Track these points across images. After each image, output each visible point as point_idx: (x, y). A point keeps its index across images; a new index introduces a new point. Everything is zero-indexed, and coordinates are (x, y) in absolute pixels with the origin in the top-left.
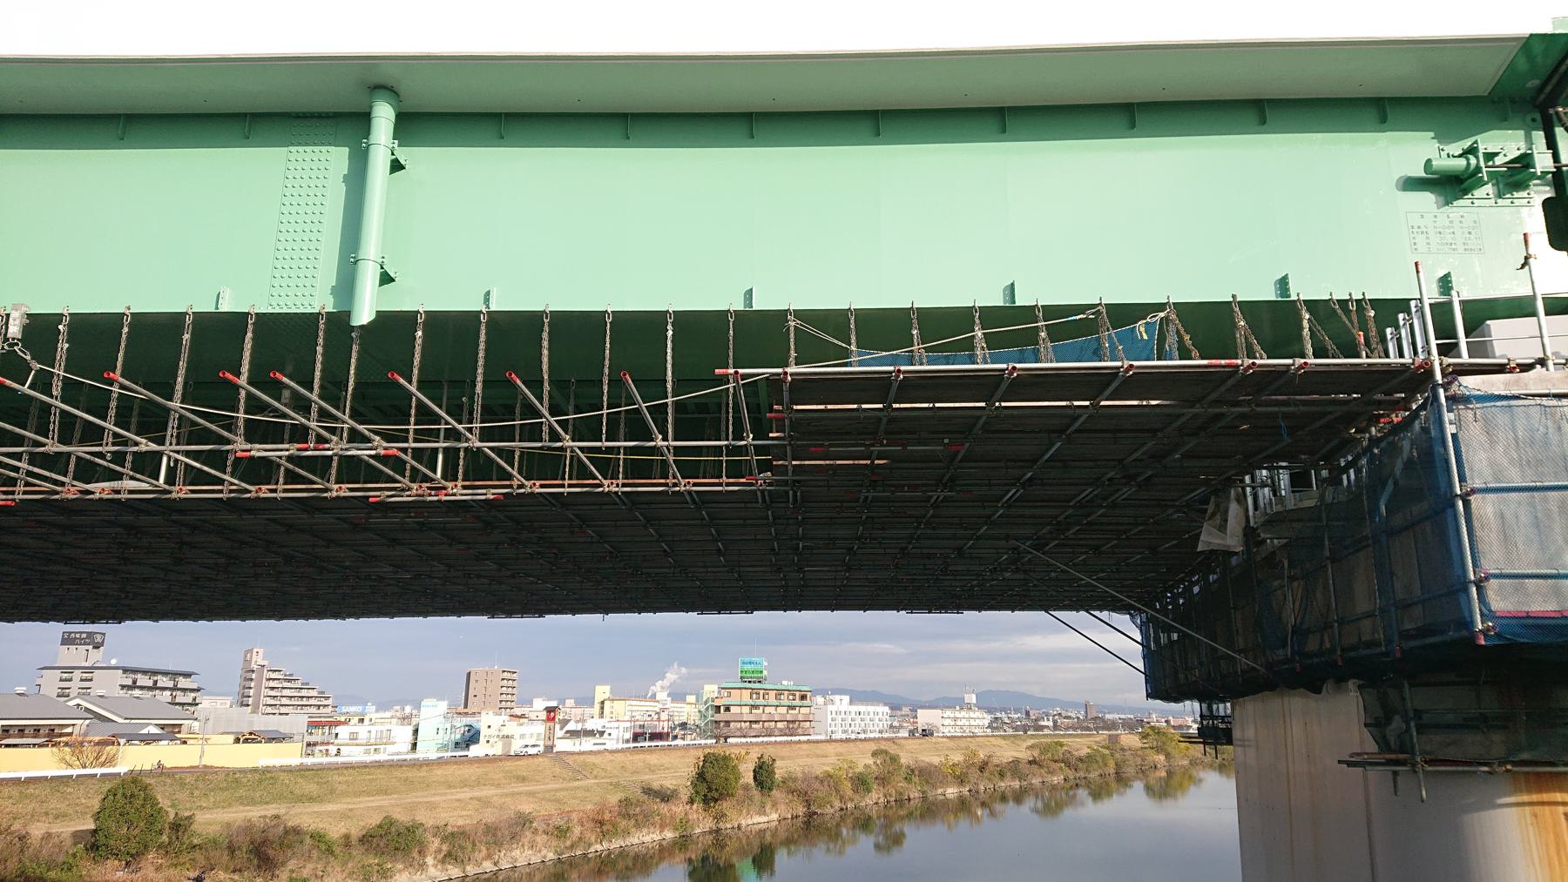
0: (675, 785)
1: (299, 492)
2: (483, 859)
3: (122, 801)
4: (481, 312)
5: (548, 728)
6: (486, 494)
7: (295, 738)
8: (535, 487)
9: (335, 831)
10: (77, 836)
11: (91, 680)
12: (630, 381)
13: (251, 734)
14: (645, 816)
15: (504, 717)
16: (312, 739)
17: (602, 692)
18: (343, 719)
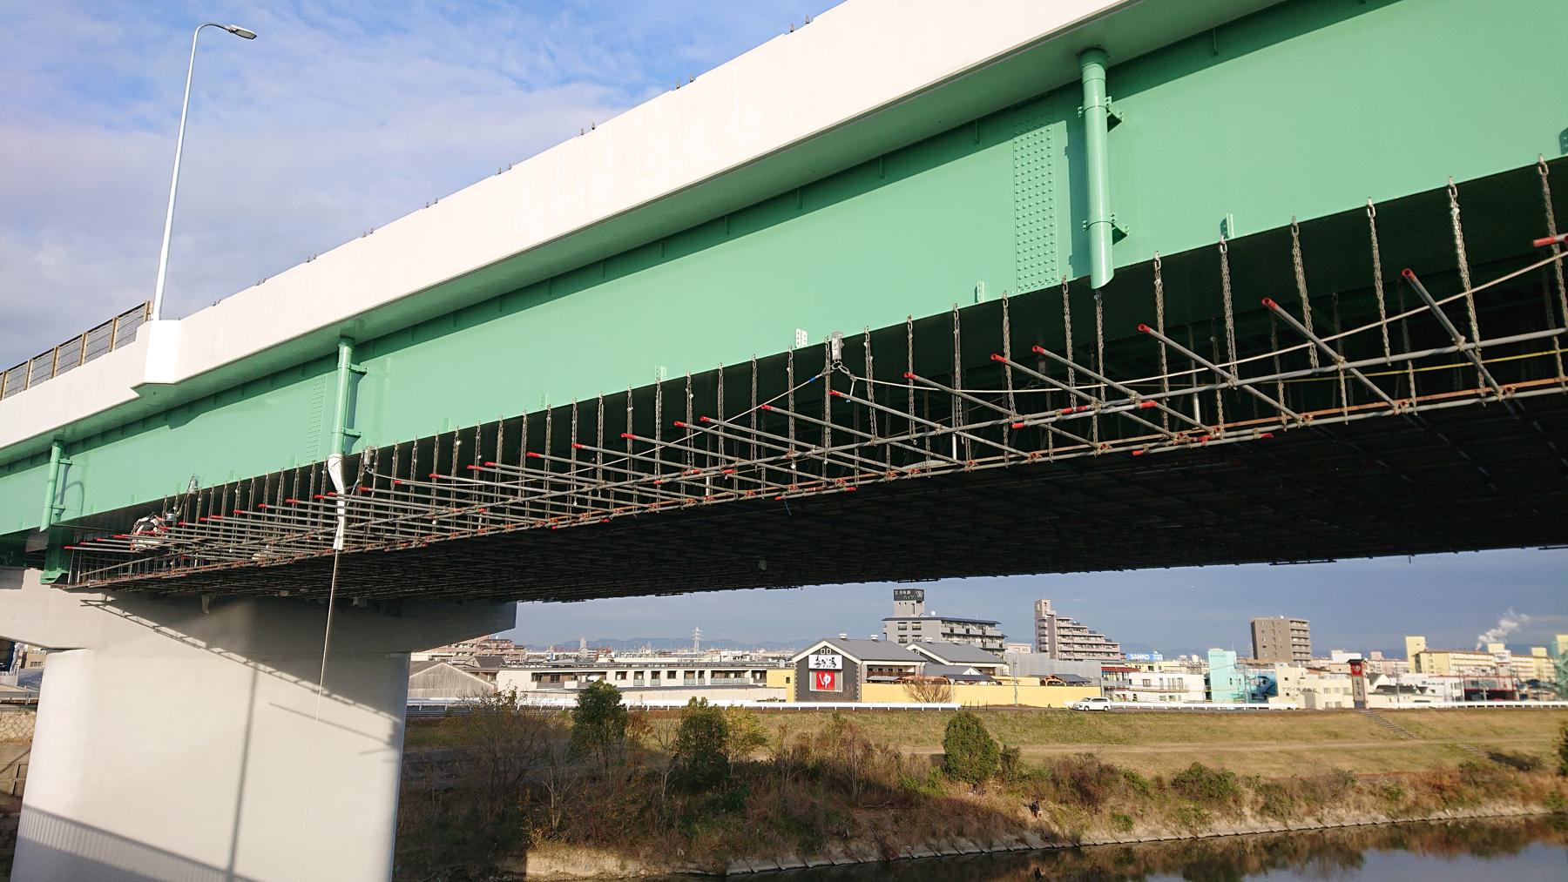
1: (1067, 453)
3: (961, 732)
5: (1355, 682)
6: (1253, 434)
7: (1093, 682)
8: (1308, 419)
9: (1147, 773)
10: (933, 757)
11: (920, 629)
12: (1416, 279)
13: (1053, 677)
14: (1498, 785)
15: (1300, 670)
16: (1108, 684)
17: (1415, 644)
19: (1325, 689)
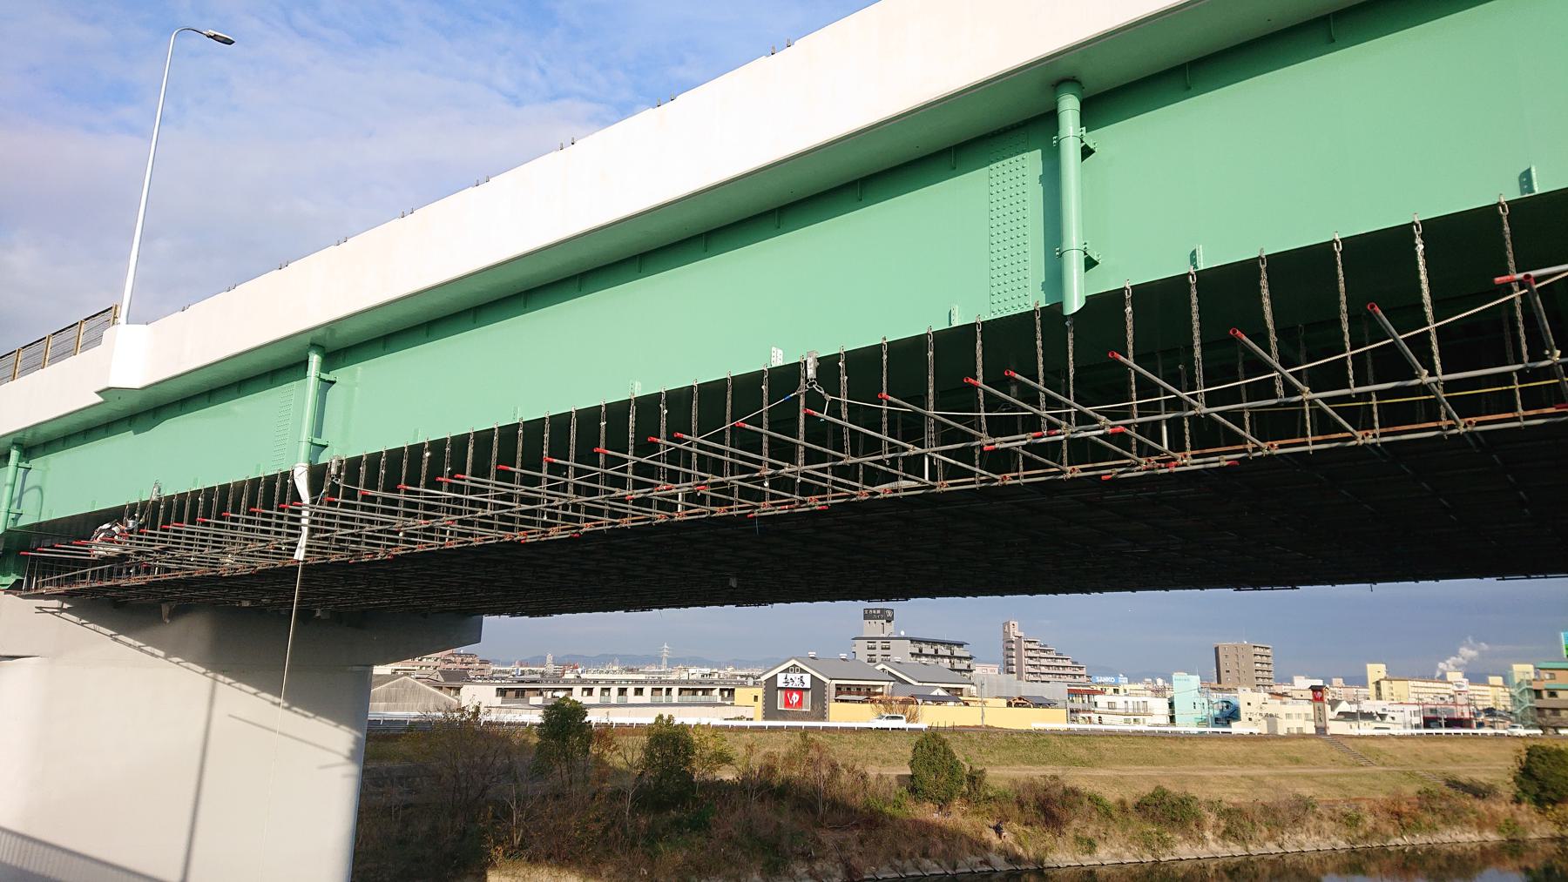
0: (1491, 780)
1: (1037, 477)
2: (1265, 839)
4: (1189, 274)
6: (1219, 461)
7: (1059, 704)
8: (1274, 448)
9: (1111, 796)
10: (899, 778)
11: (889, 649)
12: (1380, 313)
13: (1020, 699)
16: (1074, 706)
17: (1376, 671)
18: (1099, 689)
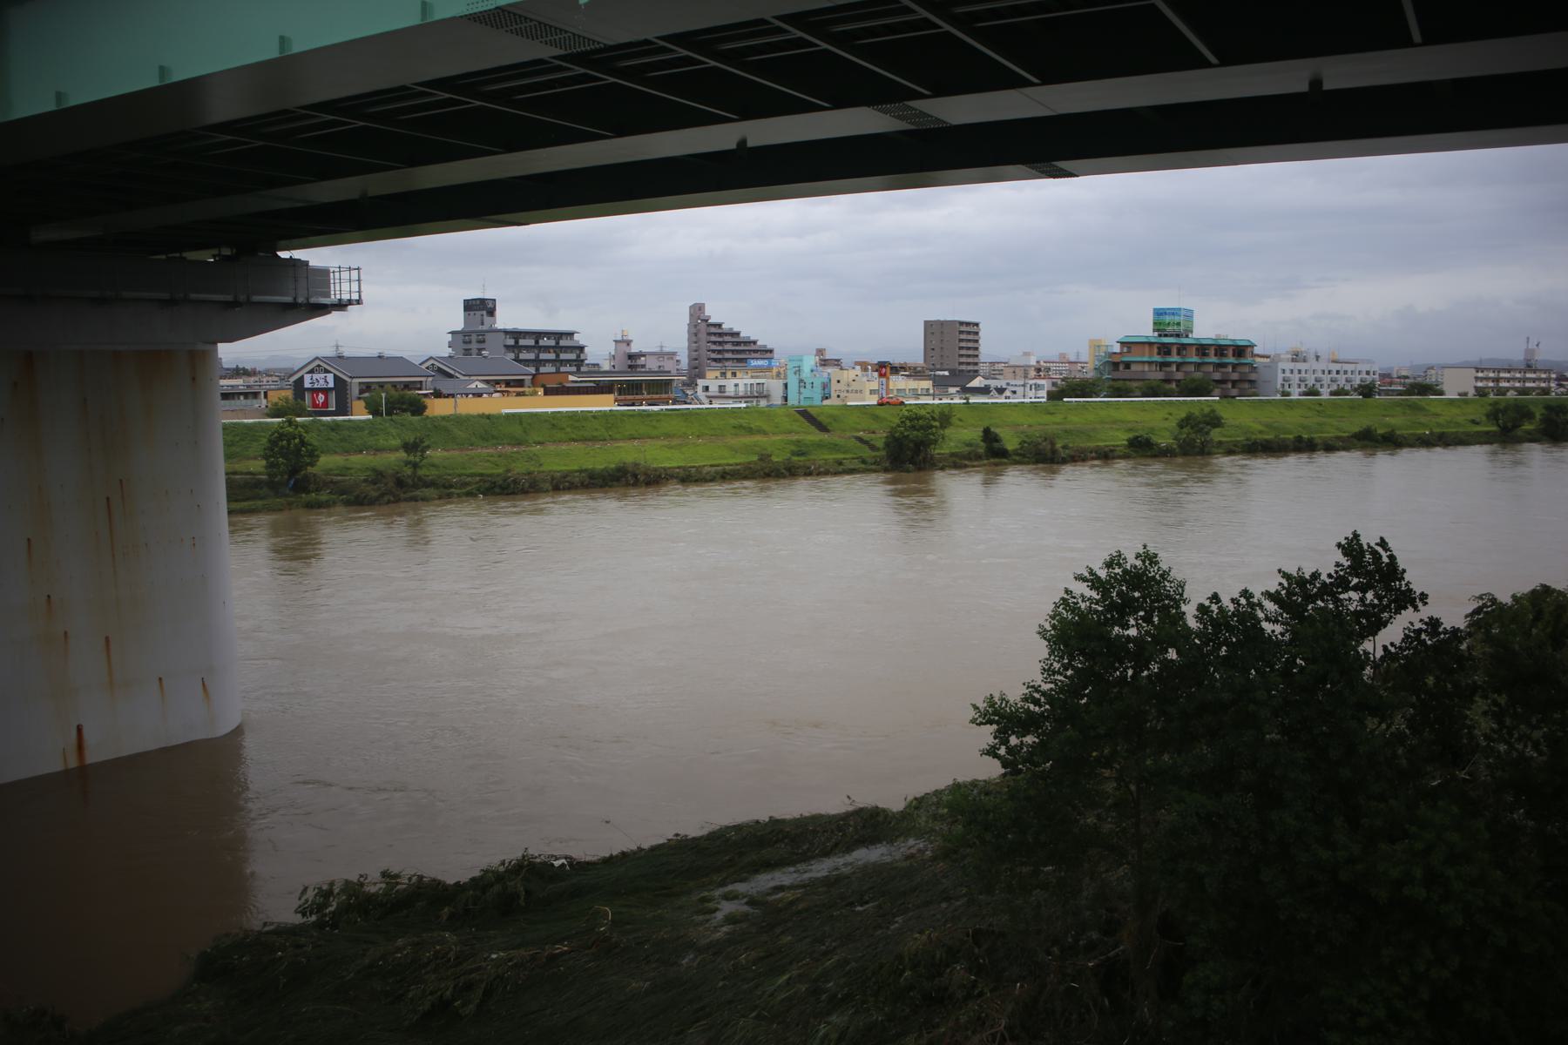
19: (871, 390)
